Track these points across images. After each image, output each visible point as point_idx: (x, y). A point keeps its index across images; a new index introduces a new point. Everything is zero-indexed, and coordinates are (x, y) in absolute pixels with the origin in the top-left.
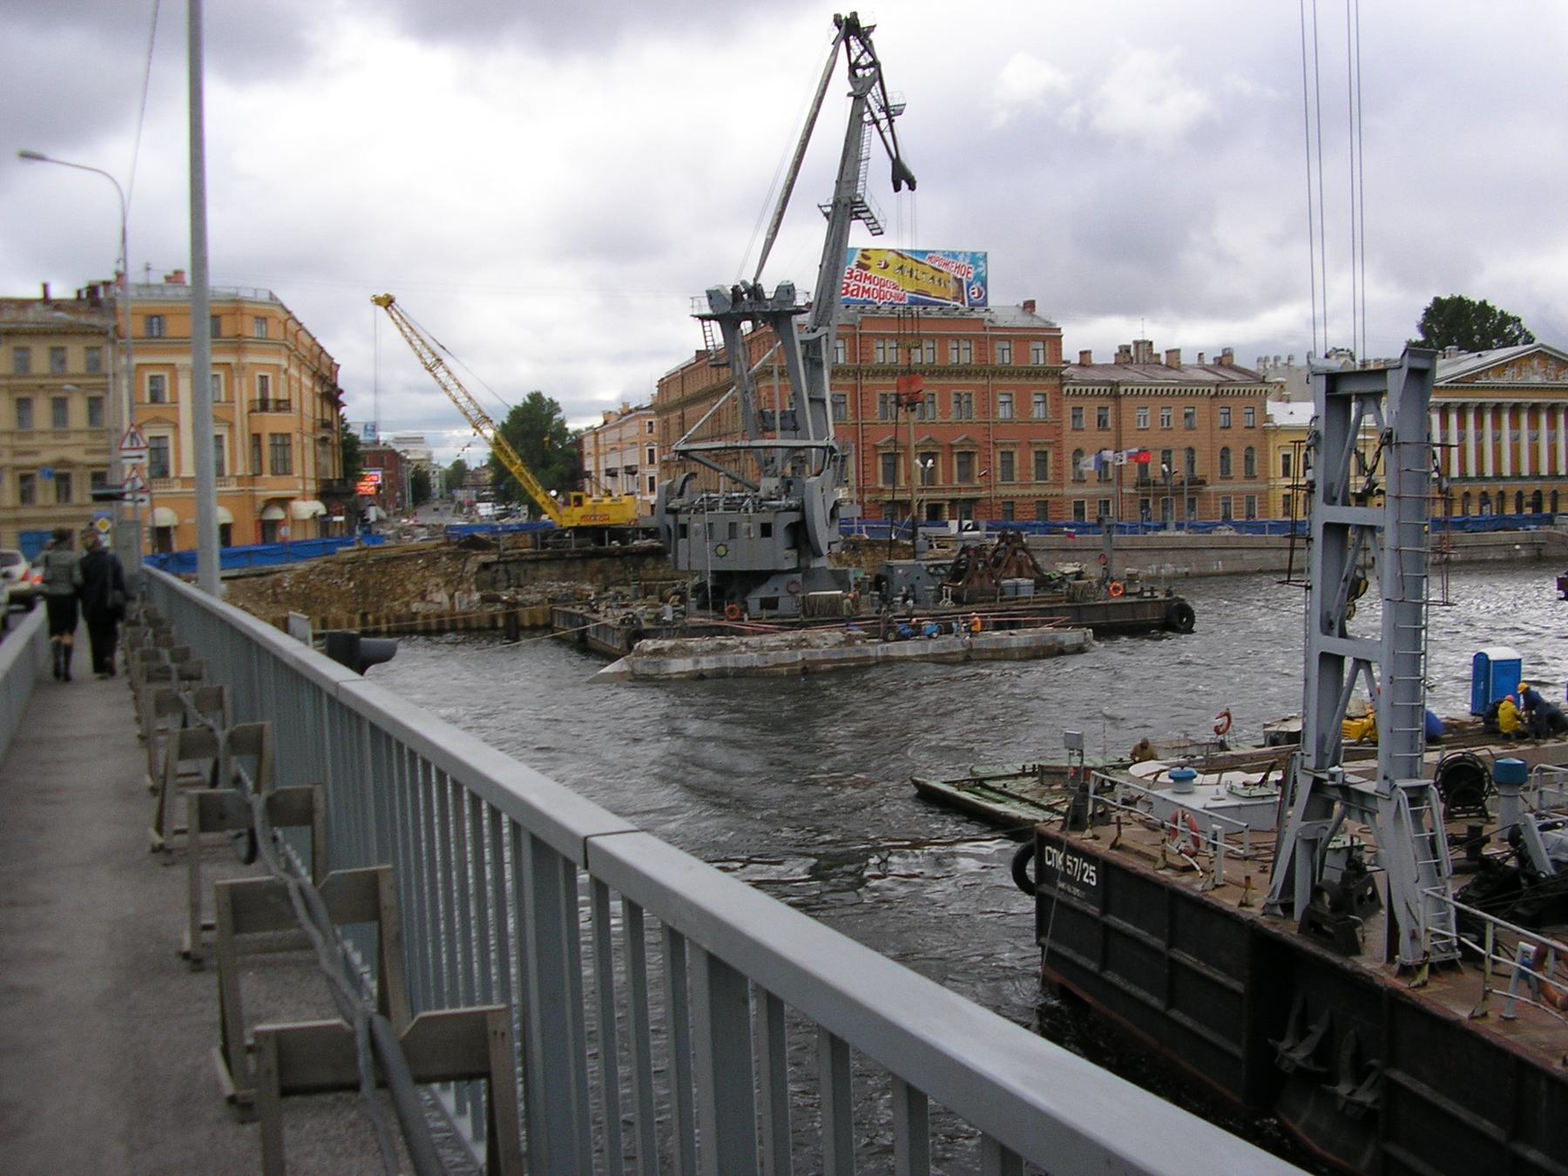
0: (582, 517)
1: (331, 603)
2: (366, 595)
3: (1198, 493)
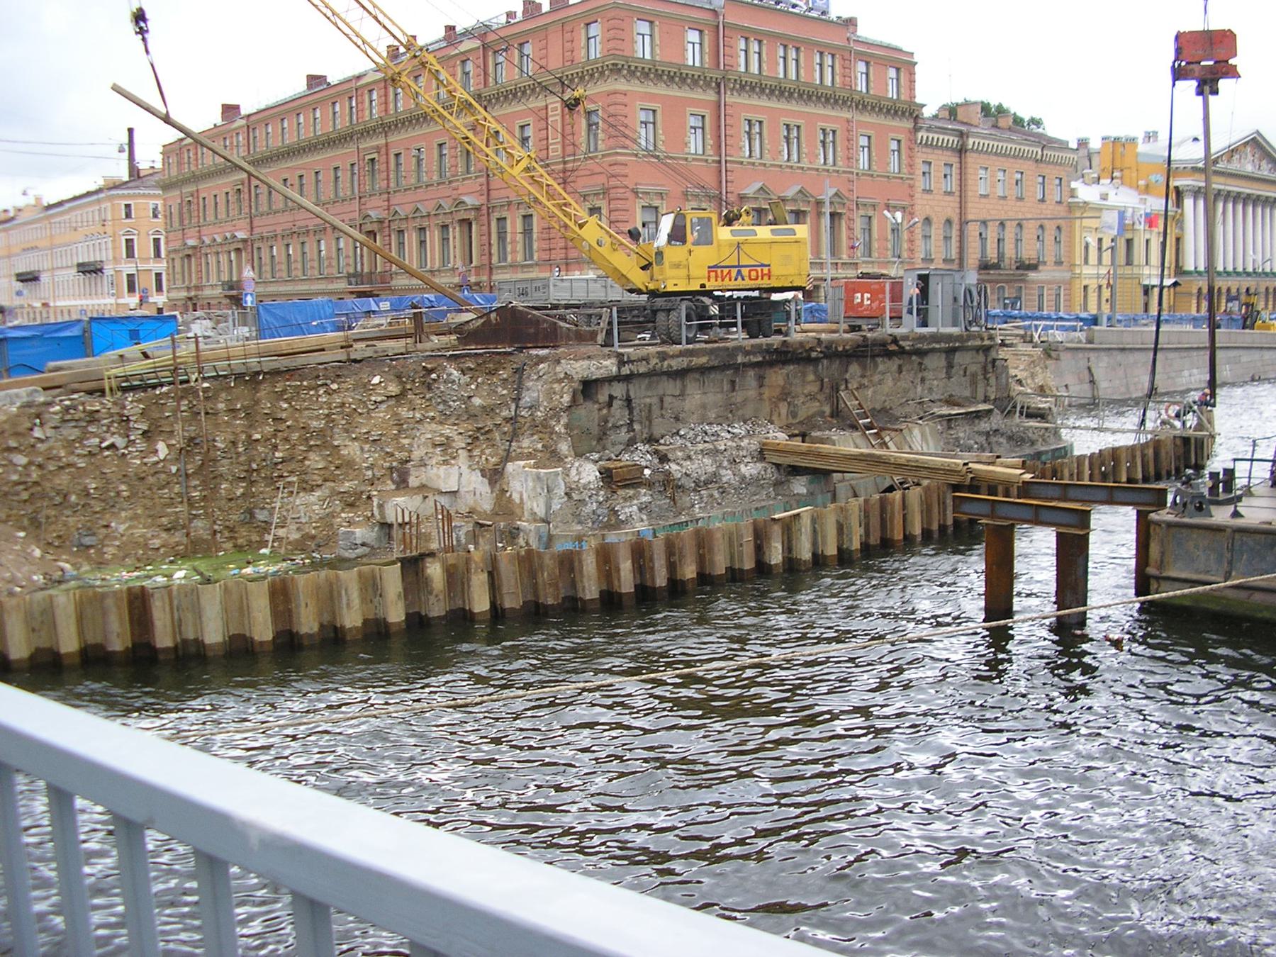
0: (712, 268)
1: (111, 505)
2: (208, 474)
3: (1024, 281)
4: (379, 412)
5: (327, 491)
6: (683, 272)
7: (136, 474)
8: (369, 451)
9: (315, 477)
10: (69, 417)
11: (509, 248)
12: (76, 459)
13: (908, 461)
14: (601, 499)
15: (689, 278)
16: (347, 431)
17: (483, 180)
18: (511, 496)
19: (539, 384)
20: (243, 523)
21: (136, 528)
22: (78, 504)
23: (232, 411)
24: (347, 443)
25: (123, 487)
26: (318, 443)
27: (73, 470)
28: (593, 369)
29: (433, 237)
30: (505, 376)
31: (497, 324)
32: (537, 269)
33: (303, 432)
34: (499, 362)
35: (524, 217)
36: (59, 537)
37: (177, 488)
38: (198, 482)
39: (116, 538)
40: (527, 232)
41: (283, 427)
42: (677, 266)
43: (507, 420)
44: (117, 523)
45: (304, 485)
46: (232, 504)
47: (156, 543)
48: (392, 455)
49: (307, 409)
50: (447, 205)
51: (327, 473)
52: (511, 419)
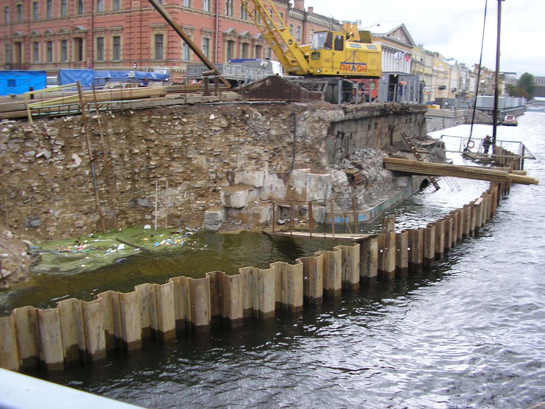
1: (48, 198)
4: (216, 137)
5: (185, 187)
6: (330, 64)
7: (63, 176)
8: (214, 162)
9: (178, 178)
10: (14, 136)
11: (105, 53)
12: (21, 165)
13: (476, 171)
14: (350, 191)
15: (333, 67)
16: (196, 149)
17: (90, 18)
18: (295, 189)
19: (305, 123)
20: (131, 208)
21: (66, 213)
22: (27, 198)
23: (117, 134)
24: (196, 156)
25: (56, 185)
26: (179, 156)
27: (19, 173)
28: (336, 116)
29: (57, 46)
30: (284, 117)
31: (270, 86)
32: (122, 64)
33: (166, 149)
34: (280, 109)
35: (114, 37)
36: (16, 221)
37: (90, 186)
38: (102, 181)
39: (53, 221)
40: (116, 45)
41: (152, 145)
42: (327, 61)
43: (289, 144)
44: (54, 210)
45: (172, 183)
46: (123, 195)
47: (81, 223)
48: (228, 164)
49: (167, 134)
50: (66, 30)
51: (186, 176)
52: (291, 143)
